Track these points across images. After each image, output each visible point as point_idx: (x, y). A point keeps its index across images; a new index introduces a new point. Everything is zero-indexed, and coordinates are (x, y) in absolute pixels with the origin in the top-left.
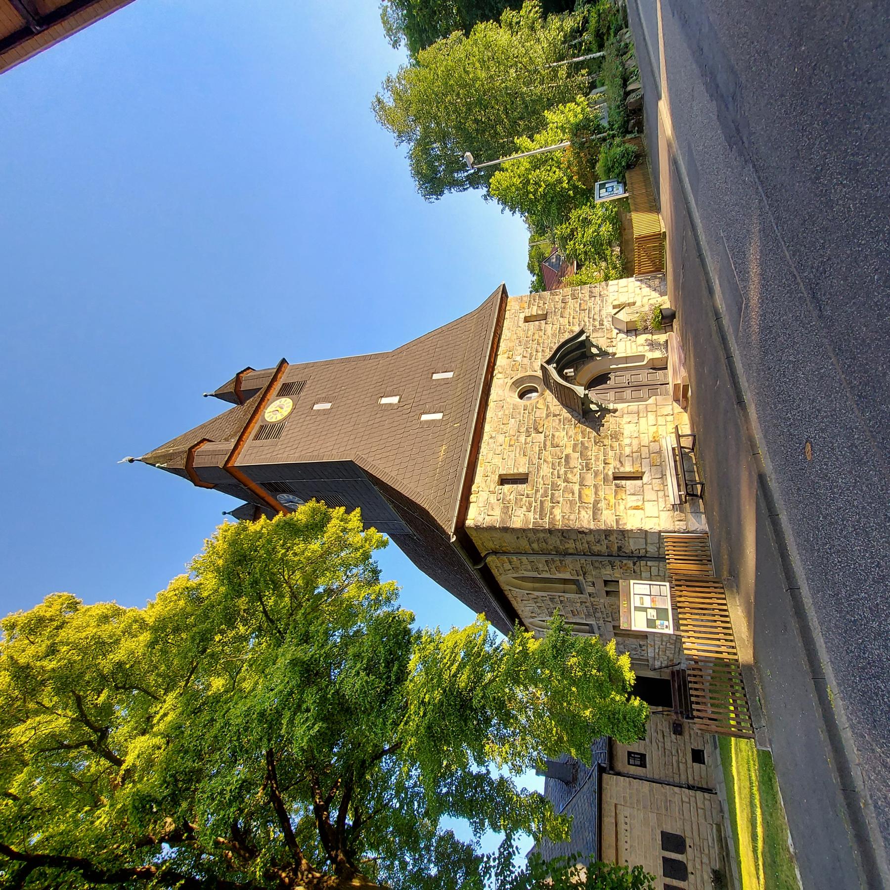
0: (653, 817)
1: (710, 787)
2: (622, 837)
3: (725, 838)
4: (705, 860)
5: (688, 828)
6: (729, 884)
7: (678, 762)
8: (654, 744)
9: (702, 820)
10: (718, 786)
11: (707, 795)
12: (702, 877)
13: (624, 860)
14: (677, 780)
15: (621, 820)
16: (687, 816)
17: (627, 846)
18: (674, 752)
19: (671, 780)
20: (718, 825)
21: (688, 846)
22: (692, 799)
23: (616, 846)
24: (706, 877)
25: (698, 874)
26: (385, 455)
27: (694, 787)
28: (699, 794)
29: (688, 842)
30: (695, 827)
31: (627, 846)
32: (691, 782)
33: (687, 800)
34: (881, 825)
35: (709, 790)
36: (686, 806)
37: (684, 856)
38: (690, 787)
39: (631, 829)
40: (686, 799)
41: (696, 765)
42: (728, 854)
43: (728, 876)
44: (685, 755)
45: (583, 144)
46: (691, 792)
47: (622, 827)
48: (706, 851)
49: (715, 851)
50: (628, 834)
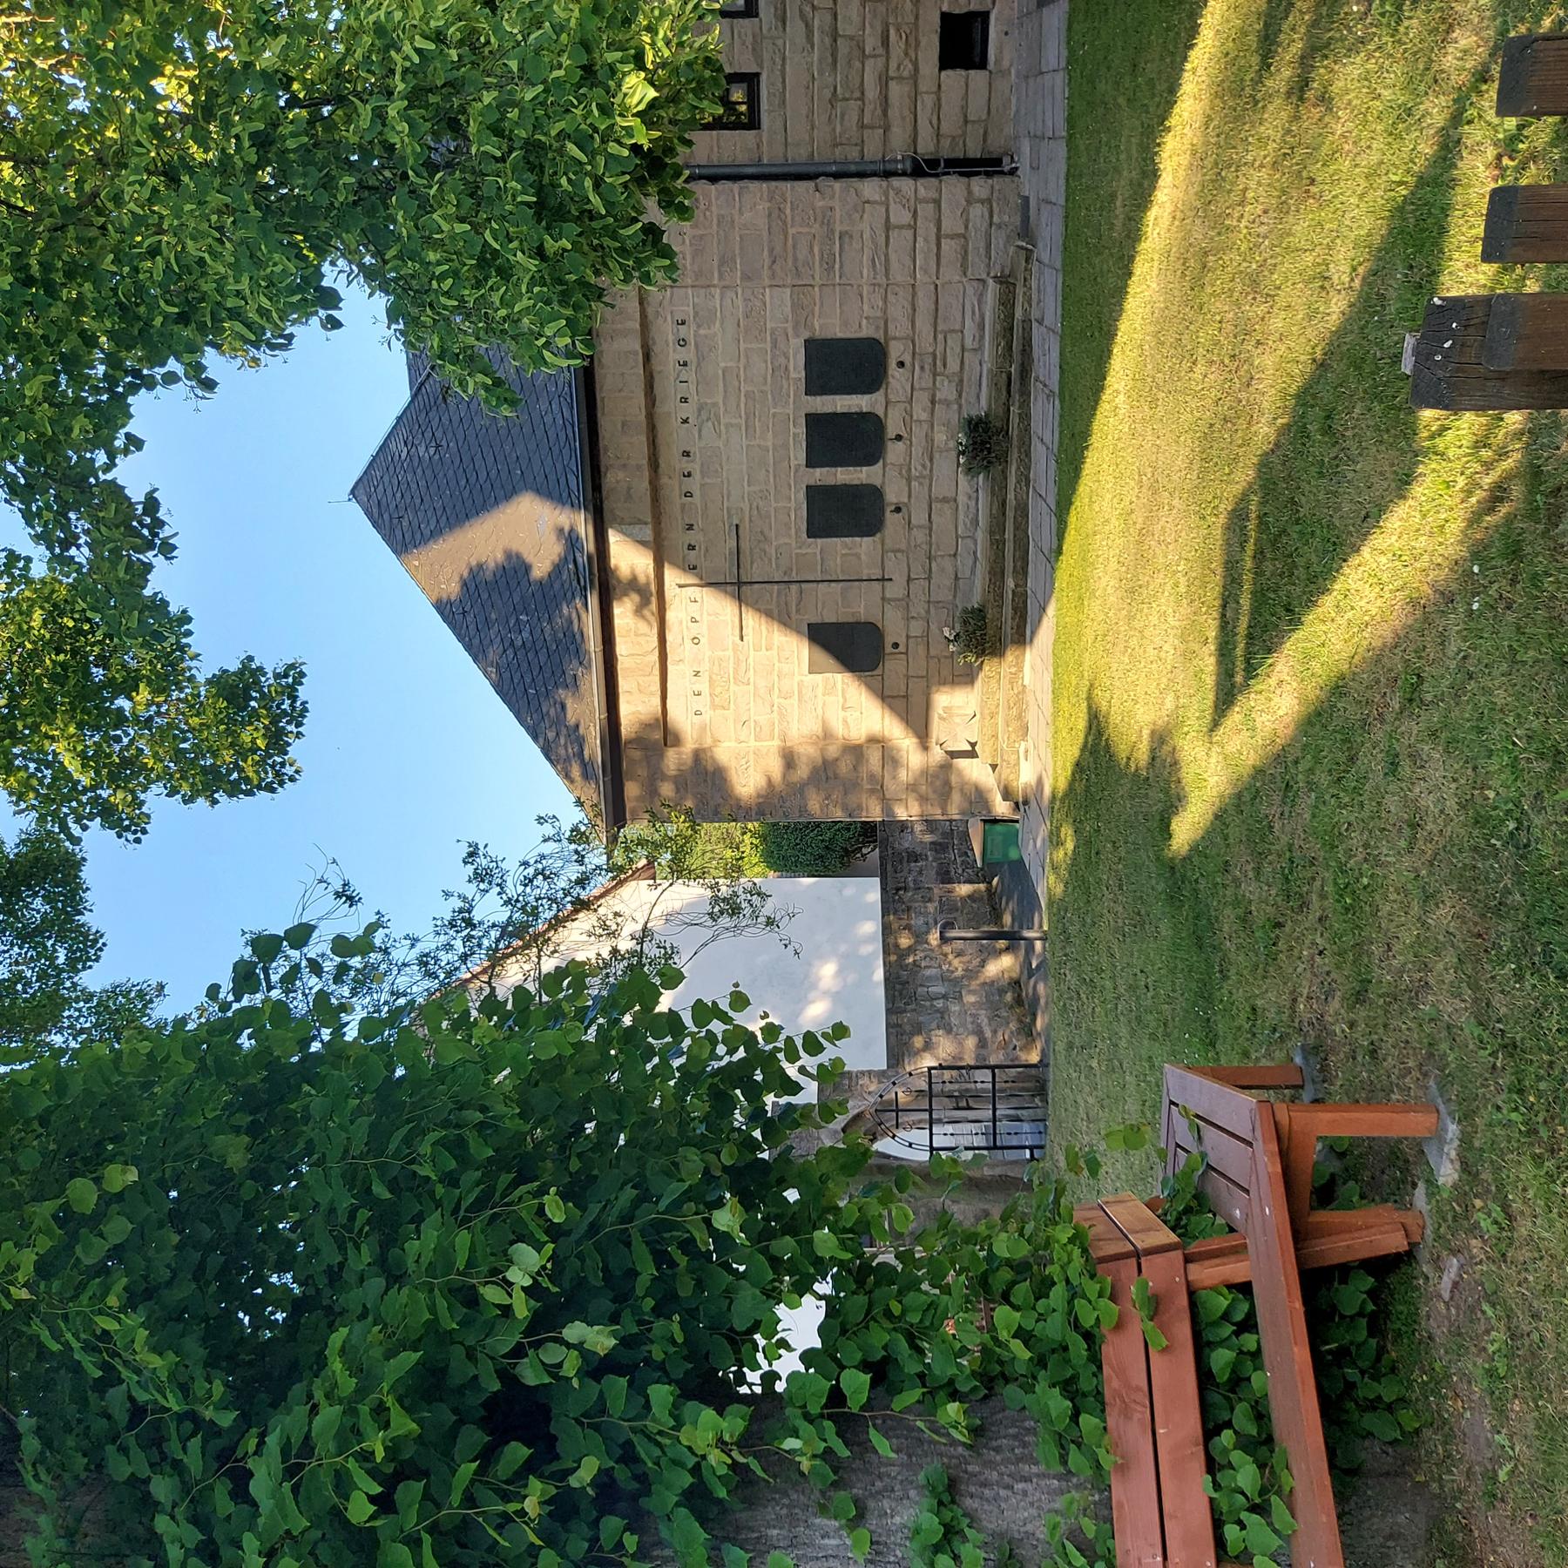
0: (778, 304)
1: (996, 145)
2: (668, 388)
3: (1027, 322)
4: (946, 391)
5: (898, 312)
6: (1014, 455)
7: (884, 80)
8: (795, 28)
9: (951, 273)
10: (1026, 146)
11: (980, 186)
12: (930, 439)
13: (676, 452)
14: (873, 150)
15: (665, 332)
16: (899, 275)
17: (687, 410)
18: (871, 42)
19: (854, 154)
20: (1006, 282)
21: (892, 364)
22: (926, 210)
23: (650, 417)
24: (940, 437)
25: (919, 433)
26: (552, 477)
27: (933, 163)
28: (953, 188)
29: (896, 351)
30: (924, 303)
31: (687, 410)
32: (926, 147)
33: (906, 218)
34: (1502, 201)
35: (989, 165)
36: (900, 239)
37: (878, 396)
38: (922, 168)
39: (701, 358)
40: (901, 216)
41: (953, 77)
42: (1025, 372)
43: (1014, 432)
44: (913, 43)
45: (1362, 1197)
46: (925, 187)
47: (669, 356)
48: (953, 365)
49: (985, 361)
50: (689, 374)
